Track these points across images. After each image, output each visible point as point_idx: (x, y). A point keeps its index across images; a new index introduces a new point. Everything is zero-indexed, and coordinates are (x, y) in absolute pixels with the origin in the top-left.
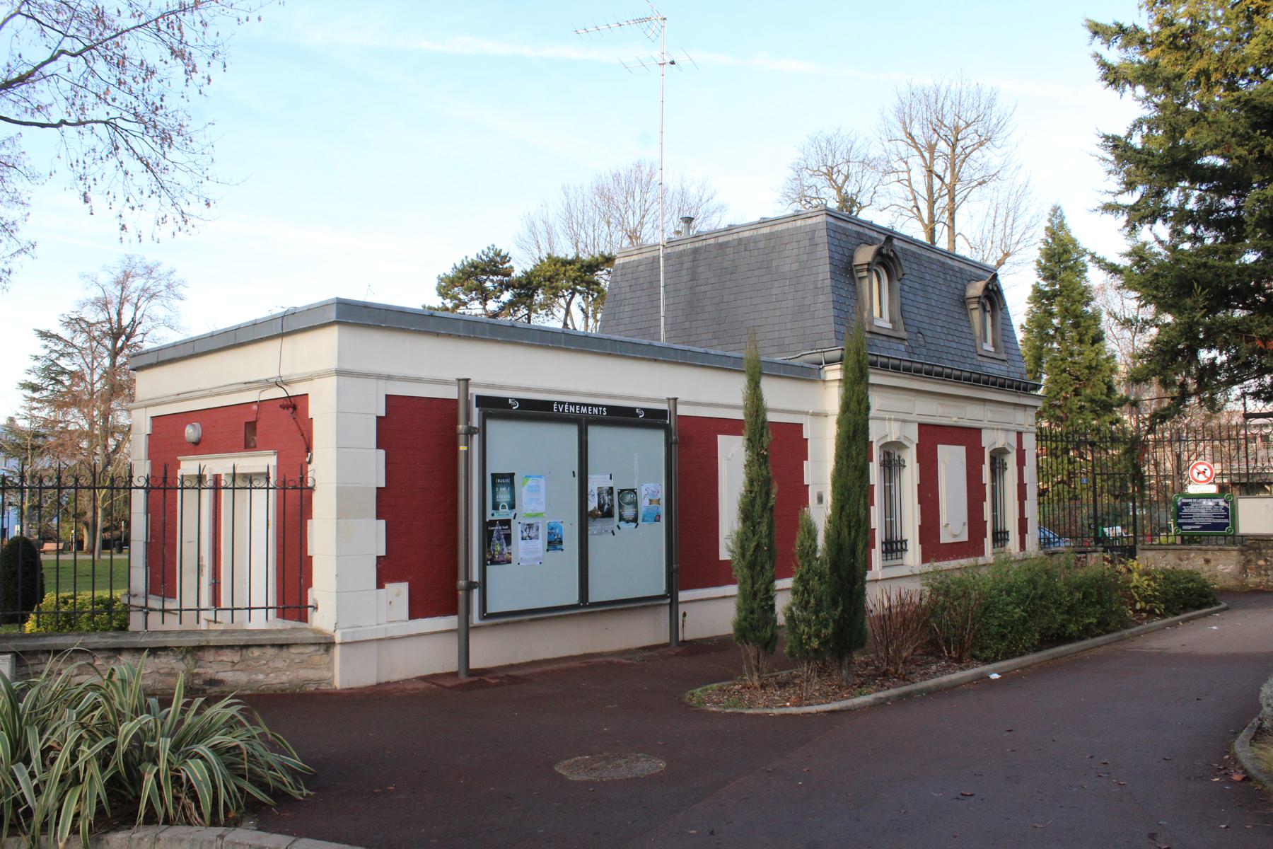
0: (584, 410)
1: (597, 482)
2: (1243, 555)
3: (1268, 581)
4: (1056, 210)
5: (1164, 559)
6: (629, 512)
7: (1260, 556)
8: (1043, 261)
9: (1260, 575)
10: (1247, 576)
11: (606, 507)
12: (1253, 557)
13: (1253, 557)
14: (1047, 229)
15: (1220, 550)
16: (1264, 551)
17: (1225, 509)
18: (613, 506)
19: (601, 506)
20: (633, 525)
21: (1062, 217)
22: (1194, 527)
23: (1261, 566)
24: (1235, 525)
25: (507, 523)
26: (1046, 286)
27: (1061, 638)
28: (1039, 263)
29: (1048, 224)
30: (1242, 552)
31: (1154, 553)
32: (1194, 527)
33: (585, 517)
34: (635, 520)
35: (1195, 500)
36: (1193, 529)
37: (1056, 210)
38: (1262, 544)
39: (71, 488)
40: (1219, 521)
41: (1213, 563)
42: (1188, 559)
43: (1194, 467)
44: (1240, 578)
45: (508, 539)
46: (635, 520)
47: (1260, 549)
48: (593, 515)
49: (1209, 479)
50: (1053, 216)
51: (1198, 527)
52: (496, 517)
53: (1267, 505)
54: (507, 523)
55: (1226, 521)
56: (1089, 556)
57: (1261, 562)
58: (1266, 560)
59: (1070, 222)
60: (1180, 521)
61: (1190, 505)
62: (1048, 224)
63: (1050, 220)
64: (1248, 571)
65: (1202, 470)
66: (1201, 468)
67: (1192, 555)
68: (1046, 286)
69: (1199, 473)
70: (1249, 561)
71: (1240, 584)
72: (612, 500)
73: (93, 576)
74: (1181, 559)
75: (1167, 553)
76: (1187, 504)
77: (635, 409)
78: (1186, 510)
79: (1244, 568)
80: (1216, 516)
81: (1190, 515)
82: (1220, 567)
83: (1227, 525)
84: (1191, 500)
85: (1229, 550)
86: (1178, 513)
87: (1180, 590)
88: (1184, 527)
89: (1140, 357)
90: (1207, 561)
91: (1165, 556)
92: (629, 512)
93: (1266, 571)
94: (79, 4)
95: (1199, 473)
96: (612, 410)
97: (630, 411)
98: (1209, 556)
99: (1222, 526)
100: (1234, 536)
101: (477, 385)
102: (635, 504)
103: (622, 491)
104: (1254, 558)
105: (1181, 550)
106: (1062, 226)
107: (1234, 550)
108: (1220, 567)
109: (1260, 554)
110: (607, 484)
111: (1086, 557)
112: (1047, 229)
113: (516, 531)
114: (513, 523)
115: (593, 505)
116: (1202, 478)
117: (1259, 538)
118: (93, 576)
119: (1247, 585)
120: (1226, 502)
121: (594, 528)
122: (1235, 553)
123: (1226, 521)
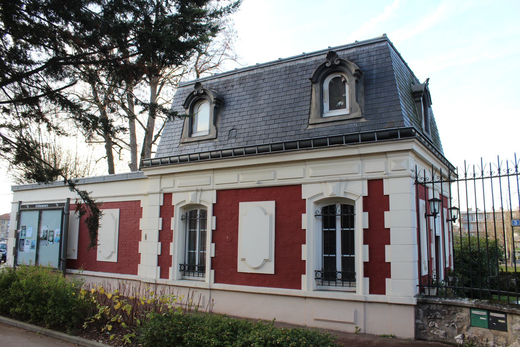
0: (43, 206)
1: (43, 228)
6: (51, 239)
11: (45, 236)
18: (47, 236)
20: (52, 243)
33: (39, 239)
34: (53, 241)
39: (430, 182)
45: (23, 244)
46: (53, 241)
48: (42, 239)
52: (22, 238)
54: (23, 240)
56: (509, 318)
72: (47, 234)
73: (468, 223)
77: (55, 204)
87: (163, 335)
92: (51, 239)
94: (56, 113)
96: (50, 205)
97: (54, 205)
101: (24, 202)
102: (53, 236)
103: (50, 231)
110: (46, 229)
111: (505, 319)
114: (25, 240)
118: (468, 223)
121: (42, 243)
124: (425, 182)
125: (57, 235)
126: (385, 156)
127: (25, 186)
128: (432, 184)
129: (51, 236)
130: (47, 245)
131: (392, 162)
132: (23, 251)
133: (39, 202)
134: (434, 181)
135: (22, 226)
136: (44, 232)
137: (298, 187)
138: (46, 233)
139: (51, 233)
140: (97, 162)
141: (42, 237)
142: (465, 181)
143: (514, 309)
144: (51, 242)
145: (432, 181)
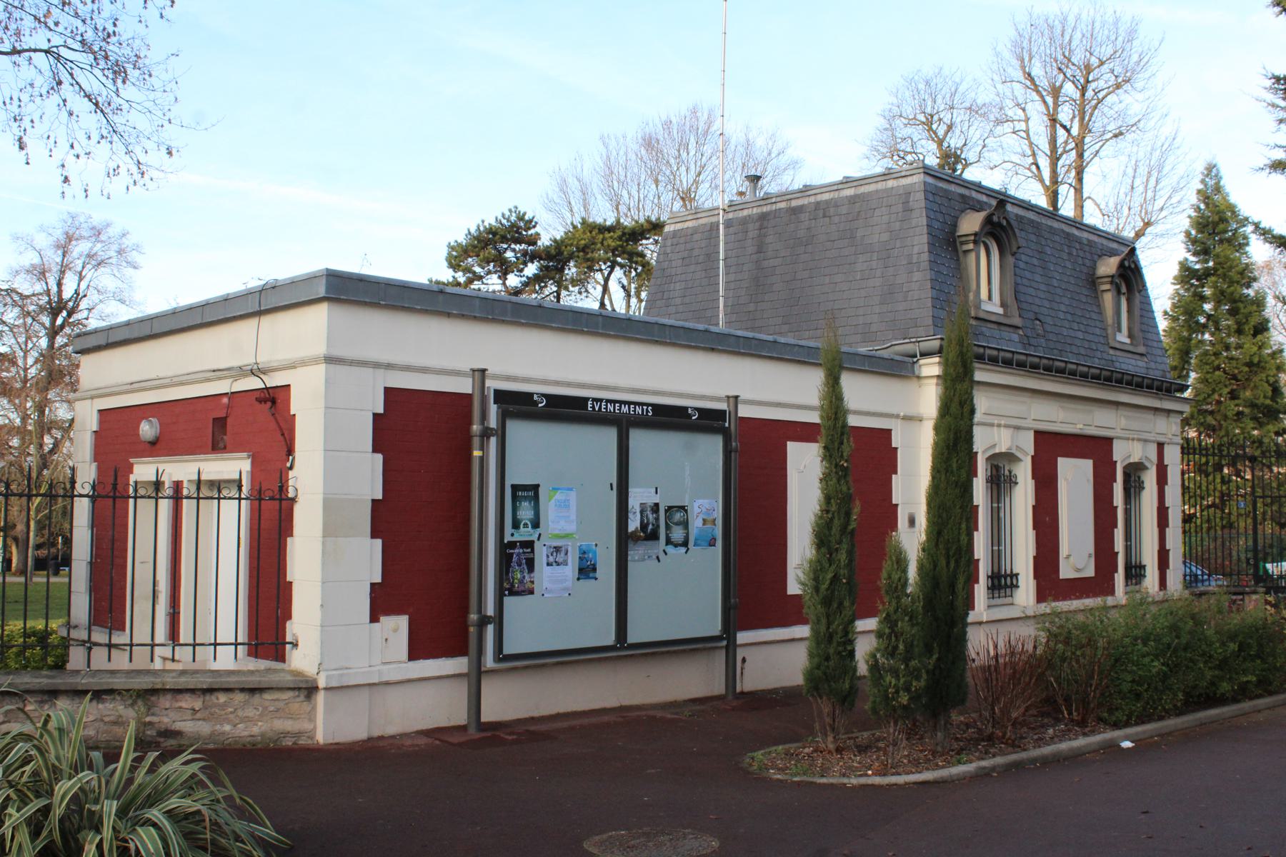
1: (639, 497)
4: (1210, 169)
6: (678, 534)
8: (1193, 232)
11: (650, 527)
19: (644, 526)
20: (683, 550)
21: (1218, 178)
25: (529, 545)
27: (1210, 699)
28: (1188, 234)
33: (624, 539)
34: (685, 544)
37: (1210, 169)
45: (530, 565)
46: (685, 544)
48: (635, 537)
54: (529, 545)
62: (1201, 187)
63: (1203, 181)
68: (1197, 262)
72: (657, 519)
77: (686, 408)
97: (681, 411)
101: (496, 377)
102: (685, 524)
103: (670, 508)
106: (1218, 189)
110: (652, 499)
112: (1199, 192)
113: (541, 554)
114: (537, 545)
115: (634, 524)
121: (635, 553)
124: (76, 496)
125: (704, 520)
126: (1115, 407)
127: (441, 297)
128: (110, 502)
129: (677, 524)
130: (658, 558)
131: (1122, 418)
132: (531, 592)
133: (615, 389)
134: (201, 495)
135: (513, 486)
136: (642, 512)
137: (1109, 441)
138: (651, 517)
139: (678, 516)
140: (28, 163)
141: (635, 532)
142: (237, 501)
143: (610, 834)
144: (676, 546)
145: (112, 494)
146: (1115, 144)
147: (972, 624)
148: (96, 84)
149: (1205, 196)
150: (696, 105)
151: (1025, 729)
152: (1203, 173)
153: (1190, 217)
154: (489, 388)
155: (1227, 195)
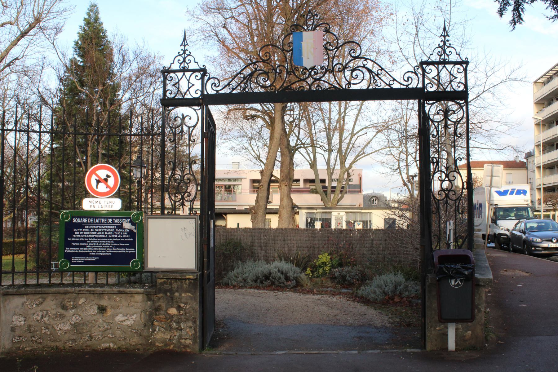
2: (149, 299)
3: (180, 337)
4: (93, 8)
5: (40, 308)
7: (172, 301)
8: (80, 42)
9: (170, 328)
10: (154, 331)
12: (163, 304)
13: (163, 304)
14: (85, 19)
15: (120, 293)
16: (177, 294)
17: (131, 232)
21: (97, 13)
22: (87, 259)
23: (172, 316)
24: (143, 261)
26: (81, 62)
28: (77, 43)
29: (87, 17)
30: (148, 296)
31: (24, 299)
32: (87, 259)
35: (91, 220)
36: (86, 263)
37: (93, 8)
38: (175, 285)
40: (122, 251)
41: (109, 312)
42: (75, 307)
43: (93, 172)
44: (145, 333)
47: (171, 291)
49: (112, 189)
50: (90, 11)
51: (93, 259)
53: (185, 229)
55: (131, 250)
57: (173, 311)
58: (179, 308)
59: (103, 18)
60: (69, 250)
61: (83, 227)
62: (87, 17)
63: (88, 14)
64: (156, 323)
65: (103, 176)
66: (102, 173)
67: (81, 301)
68: (81, 62)
69: (98, 182)
70: (157, 309)
71: (143, 342)
74: (65, 308)
75: (44, 299)
76: (81, 226)
78: (77, 234)
79: (150, 322)
80: (118, 244)
81: (83, 242)
82: (120, 318)
83: (133, 256)
84: (85, 220)
85: (132, 294)
86: (66, 240)
88: (75, 259)
89: (282, 273)
90: (102, 309)
91: (41, 303)
93: (178, 323)
95: (98, 182)
98: (104, 302)
99: (126, 258)
100: (141, 271)
104: (164, 305)
105: (65, 293)
106: (97, 20)
107: (138, 293)
108: (120, 318)
109: (172, 298)
112: (85, 19)
116: (102, 188)
117: (172, 276)
119: (153, 344)
120: (133, 223)
122: (139, 298)
123: (131, 250)
146: (324, 136)
147: (299, 151)
148: (222, 32)
149: (88, 22)
150: (271, 203)
151: (347, 73)
152: (88, 9)
153: (79, 33)
154: (330, 213)
155: (102, 24)
